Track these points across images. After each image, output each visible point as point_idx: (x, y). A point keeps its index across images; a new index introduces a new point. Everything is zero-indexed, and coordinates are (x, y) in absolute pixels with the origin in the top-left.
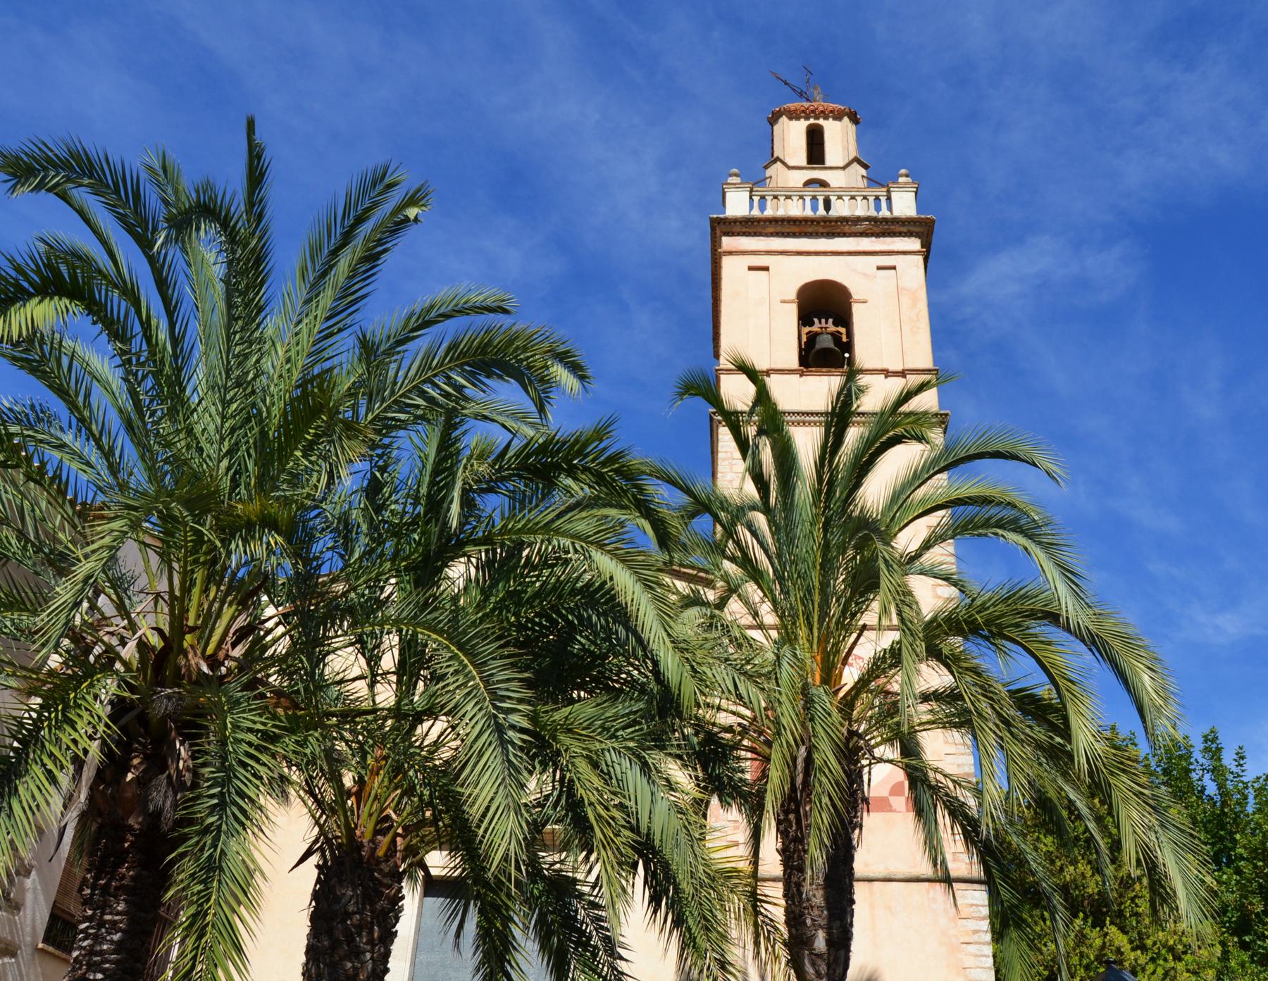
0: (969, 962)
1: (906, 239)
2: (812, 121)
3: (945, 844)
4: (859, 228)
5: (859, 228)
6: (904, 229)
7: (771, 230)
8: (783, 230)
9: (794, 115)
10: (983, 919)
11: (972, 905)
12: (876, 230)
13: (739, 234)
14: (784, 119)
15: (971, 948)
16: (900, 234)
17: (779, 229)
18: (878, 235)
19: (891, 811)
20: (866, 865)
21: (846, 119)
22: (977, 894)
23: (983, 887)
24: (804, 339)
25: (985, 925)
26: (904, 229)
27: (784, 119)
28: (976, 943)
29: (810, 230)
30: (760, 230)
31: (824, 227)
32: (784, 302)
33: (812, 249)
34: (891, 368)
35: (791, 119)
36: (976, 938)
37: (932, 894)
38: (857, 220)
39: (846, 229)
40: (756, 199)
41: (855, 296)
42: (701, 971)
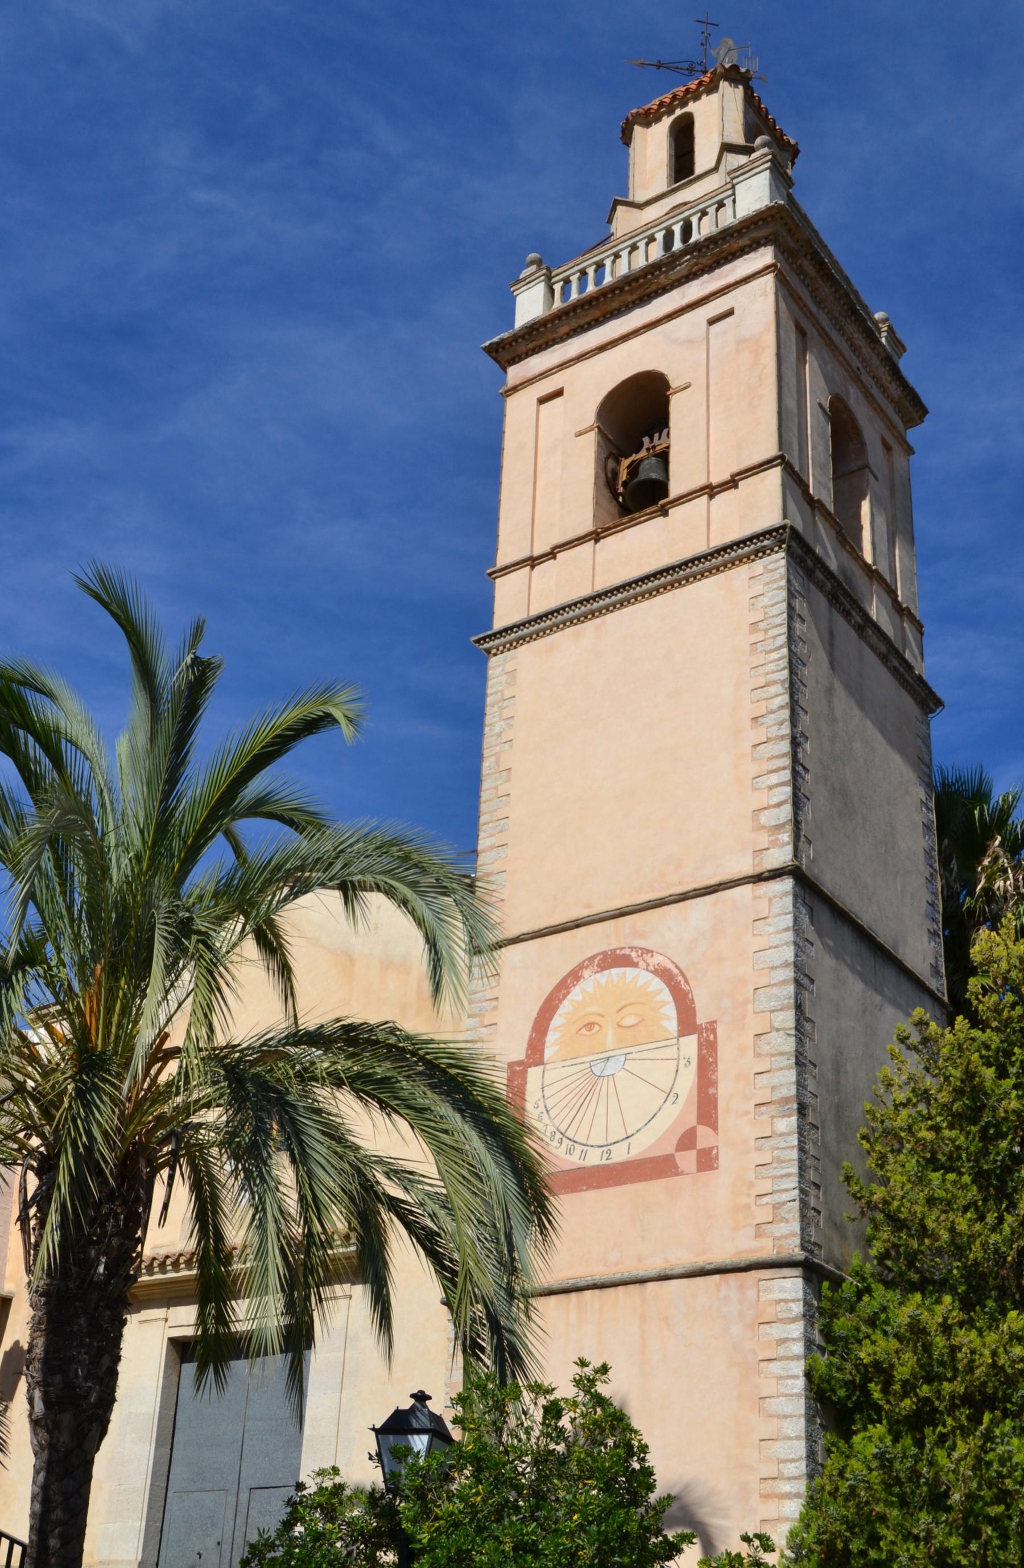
0: (769, 1387)
1: (752, 255)
2: (678, 112)
3: (752, 1193)
4: (681, 269)
5: (681, 269)
6: (744, 242)
7: (564, 329)
8: (582, 321)
9: (649, 119)
10: (794, 1320)
11: (779, 1301)
12: (704, 261)
13: (527, 355)
14: (637, 129)
15: (775, 1367)
16: (743, 252)
17: (574, 323)
18: (709, 269)
19: (677, 1174)
20: (640, 1260)
21: (724, 85)
22: (788, 1283)
23: (797, 1272)
24: (610, 475)
25: (797, 1329)
26: (744, 242)
27: (637, 129)
28: (782, 1359)
29: (615, 305)
30: (550, 336)
31: (631, 292)
32: (580, 434)
33: (616, 335)
34: (715, 480)
35: (648, 125)
36: (781, 1351)
37: (723, 1292)
38: (653, 269)
39: (663, 280)
40: (557, 287)
41: (674, 384)
42: (818, 731)
